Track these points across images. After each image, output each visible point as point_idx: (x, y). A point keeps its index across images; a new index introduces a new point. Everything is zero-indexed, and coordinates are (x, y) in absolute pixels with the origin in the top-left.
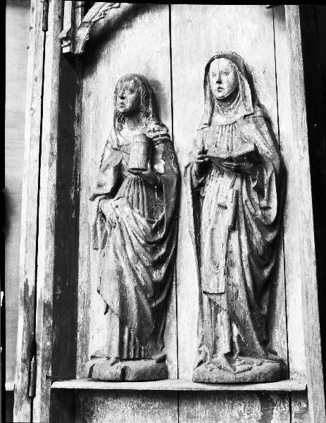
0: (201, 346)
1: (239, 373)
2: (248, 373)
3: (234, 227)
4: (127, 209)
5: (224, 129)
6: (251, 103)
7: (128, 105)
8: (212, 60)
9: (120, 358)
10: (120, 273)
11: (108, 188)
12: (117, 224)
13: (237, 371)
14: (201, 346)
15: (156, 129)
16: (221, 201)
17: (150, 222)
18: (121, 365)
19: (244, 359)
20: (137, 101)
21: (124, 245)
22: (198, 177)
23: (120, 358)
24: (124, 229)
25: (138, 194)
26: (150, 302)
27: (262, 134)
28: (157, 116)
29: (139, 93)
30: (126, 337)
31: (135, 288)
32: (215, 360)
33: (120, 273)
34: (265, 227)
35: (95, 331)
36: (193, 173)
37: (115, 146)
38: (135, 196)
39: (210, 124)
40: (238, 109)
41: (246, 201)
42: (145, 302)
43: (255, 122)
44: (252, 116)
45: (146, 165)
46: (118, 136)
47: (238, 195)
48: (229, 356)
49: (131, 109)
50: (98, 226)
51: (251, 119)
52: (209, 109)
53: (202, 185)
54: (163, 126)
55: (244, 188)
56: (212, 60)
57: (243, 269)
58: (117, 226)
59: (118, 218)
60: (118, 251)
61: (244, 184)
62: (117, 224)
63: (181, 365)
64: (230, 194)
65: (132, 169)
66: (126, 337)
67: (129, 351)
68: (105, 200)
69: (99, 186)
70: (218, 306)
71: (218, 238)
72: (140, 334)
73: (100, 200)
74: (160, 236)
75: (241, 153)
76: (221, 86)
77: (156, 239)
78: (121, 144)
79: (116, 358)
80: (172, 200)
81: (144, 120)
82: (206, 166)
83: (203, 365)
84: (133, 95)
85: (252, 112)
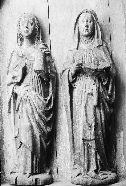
0: (74, 165)
1: (102, 179)
2: (107, 179)
3: (98, 106)
4: (33, 92)
5: (86, 52)
6: (101, 39)
7: (30, 33)
8: (82, 13)
9: (32, 174)
10: (32, 128)
11: (18, 79)
12: (28, 100)
13: (101, 179)
14: (74, 165)
15: (44, 47)
16: (90, 91)
17: (46, 100)
18: (35, 177)
19: (103, 172)
20: (34, 30)
21: (33, 112)
22: (73, 77)
23: (32, 174)
24: (32, 104)
25: (38, 83)
26: (46, 142)
27: (107, 56)
28: (43, 40)
29: (35, 25)
30: (35, 162)
31: (40, 136)
32: (88, 173)
33: (32, 128)
34: (111, 105)
35: (8, 158)
36: (70, 75)
37: (21, 55)
38: (36, 85)
39: (78, 48)
40: (93, 42)
41: (102, 92)
42: (44, 143)
43: (104, 50)
44: (101, 46)
45: (44, 69)
46: (21, 49)
47: (98, 89)
48: (96, 171)
49: (31, 34)
50: (12, 101)
51: (101, 48)
52: (77, 40)
53: (74, 81)
54: (46, 46)
55: (100, 85)
56: (82, 13)
57: (29, 118)
58: (28, 102)
59: (28, 97)
60: (29, 116)
61: (100, 83)
62: (28, 100)
63: (59, 174)
64: (95, 88)
65: (38, 71)
66: (35, 162)
67: (36, 169)
68: (17, 86)
69: (14, 78)
70: (90, 146)
71: (89, 111)
72: (41, 159)
73: (14, 86)
74: (50, 107)
75: (103, 67)
76: (26, 41)
77: (49, 109)
78: (24, 54)
79: (30, 174)
80: (55, 87)
81: (37, 41)
82: (79, 72)
83: (80, 176)
84: (33, 26)
85: (102, 44)
